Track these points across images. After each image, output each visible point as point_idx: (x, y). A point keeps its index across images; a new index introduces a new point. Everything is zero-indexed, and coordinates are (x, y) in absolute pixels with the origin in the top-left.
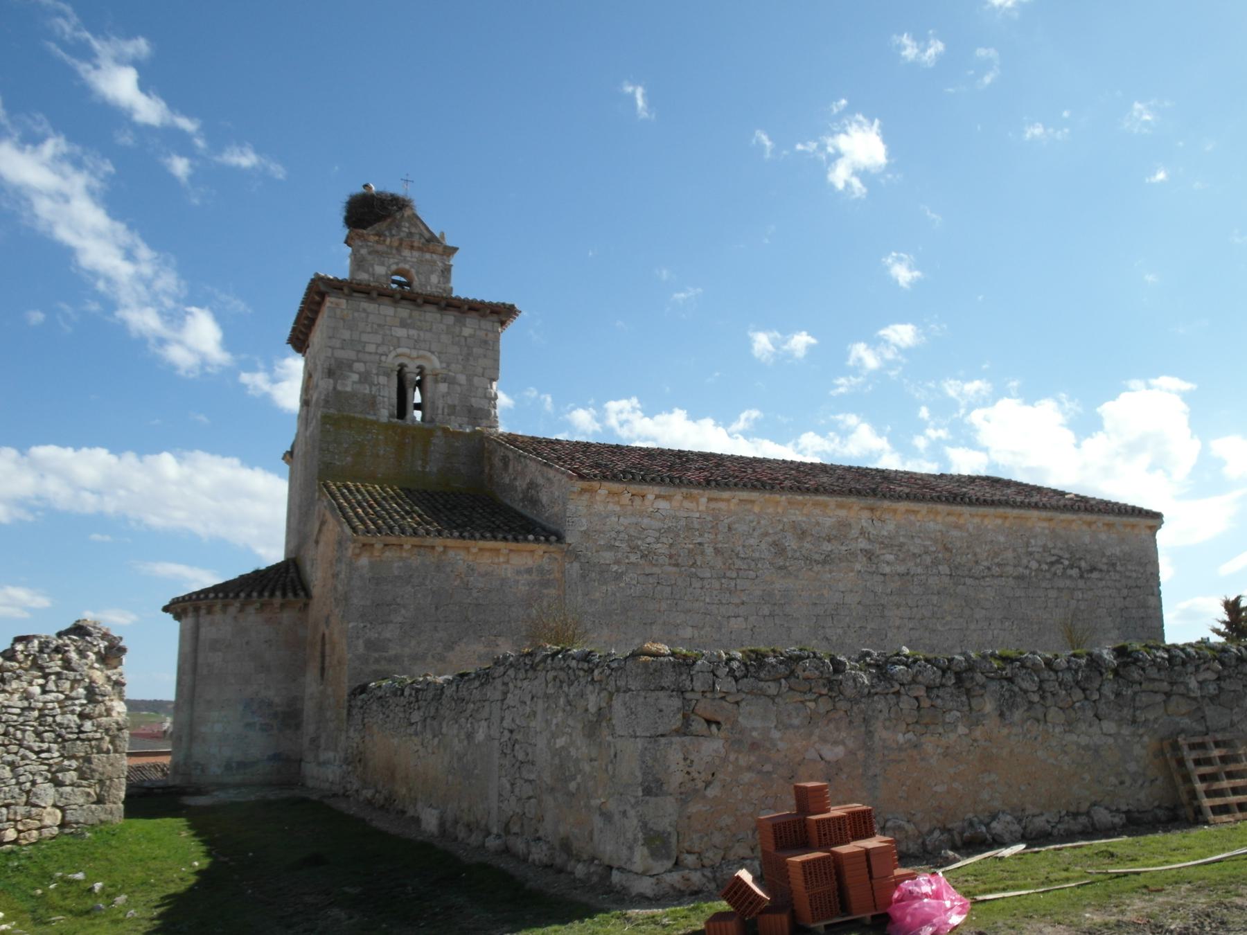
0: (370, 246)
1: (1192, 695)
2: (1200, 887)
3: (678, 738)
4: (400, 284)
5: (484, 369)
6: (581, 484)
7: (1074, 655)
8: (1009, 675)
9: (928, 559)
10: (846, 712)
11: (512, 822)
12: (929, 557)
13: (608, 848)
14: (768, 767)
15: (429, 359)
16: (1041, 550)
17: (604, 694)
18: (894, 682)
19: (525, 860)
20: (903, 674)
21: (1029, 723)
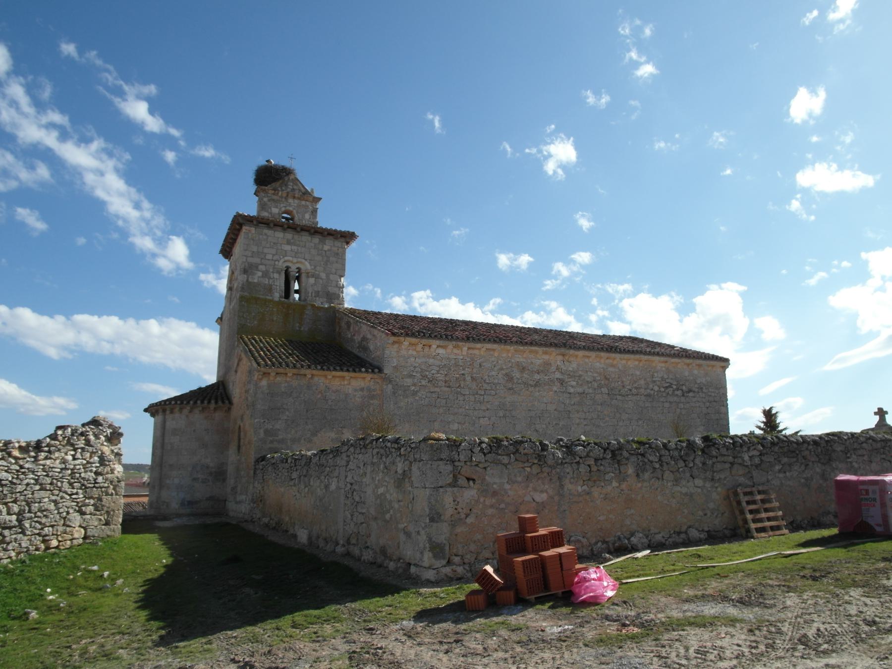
1: (746, 464)
4: (287, 219)
5: (336, 270)
6: (393, 339)
7: (679, 441)
8: (642, 452)
10: (548, 473)
14: (502, 506)
16: (660, 379)
17: (407, 462)
19: (359, 560)
21: (653, 480)
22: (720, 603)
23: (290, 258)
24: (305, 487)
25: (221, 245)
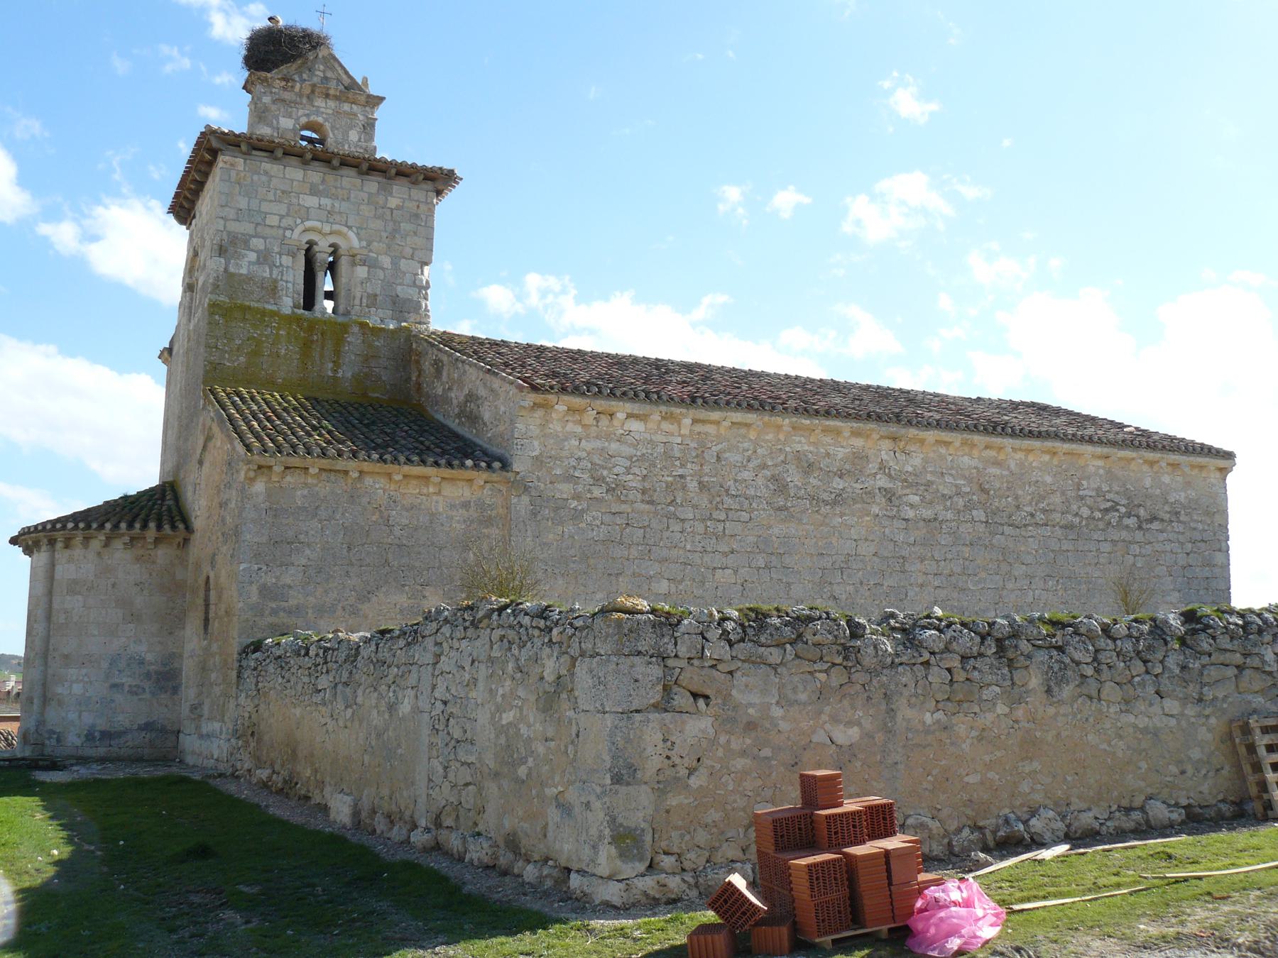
1: (1267, 669)
2: (1271, 894)
3: (657, 714)
4: (310, 140)
6: (532, 398)
7: (1136, 621)
8: (1060, 643)
9: (961, 502)
10: (864, 685)
11: (444, 813)
13: (566, 847)
14: (767, 752)
15: (345, 236)
17: (565, 658)
18: (922, 650)
19: (461, 859)
20: (934, 641)
21: (1080, 700)
22: (1213, 952)
24: (346, 707)
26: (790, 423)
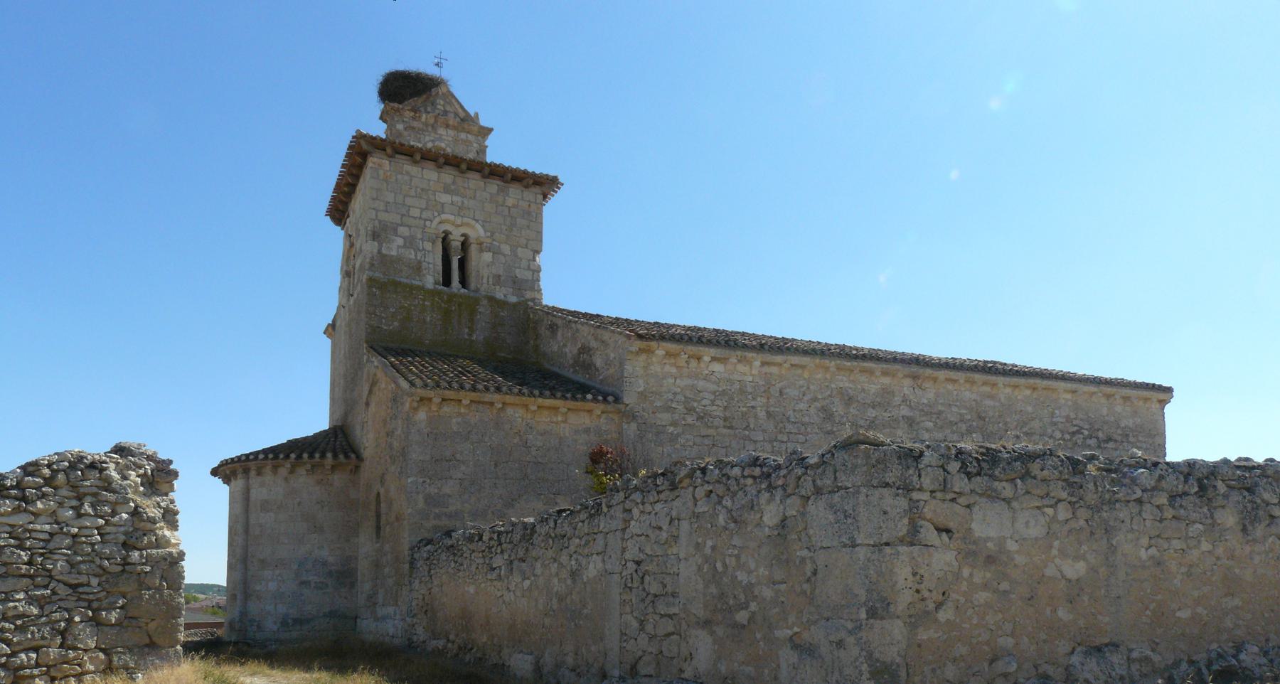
0: (406, 122)
5: (528, 240)
6: (638, 344)
9: (964, 427)
10: (1087, 521)
12: (964, 425)
14: (1005, 586)
15: (473, 227)
16: (1064, 420)
23: (452, 218)
24: (523, 580)
25: (329, 198)
26: (836, 364)
